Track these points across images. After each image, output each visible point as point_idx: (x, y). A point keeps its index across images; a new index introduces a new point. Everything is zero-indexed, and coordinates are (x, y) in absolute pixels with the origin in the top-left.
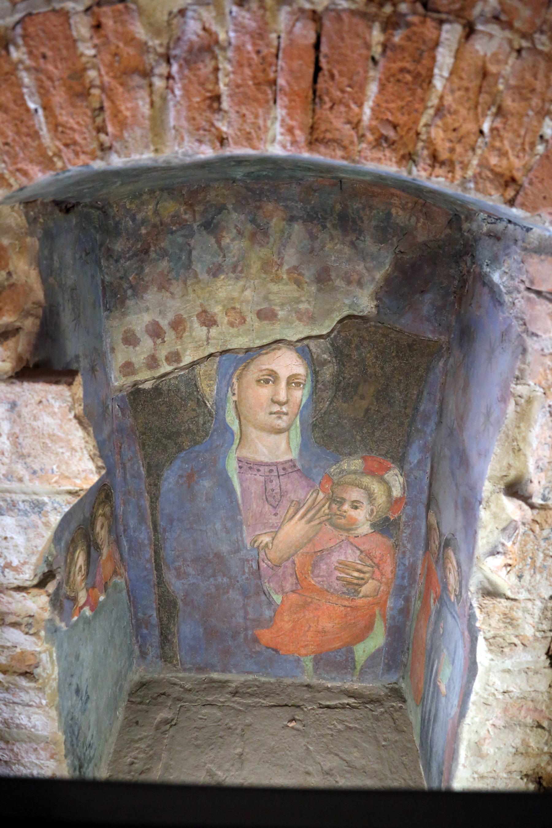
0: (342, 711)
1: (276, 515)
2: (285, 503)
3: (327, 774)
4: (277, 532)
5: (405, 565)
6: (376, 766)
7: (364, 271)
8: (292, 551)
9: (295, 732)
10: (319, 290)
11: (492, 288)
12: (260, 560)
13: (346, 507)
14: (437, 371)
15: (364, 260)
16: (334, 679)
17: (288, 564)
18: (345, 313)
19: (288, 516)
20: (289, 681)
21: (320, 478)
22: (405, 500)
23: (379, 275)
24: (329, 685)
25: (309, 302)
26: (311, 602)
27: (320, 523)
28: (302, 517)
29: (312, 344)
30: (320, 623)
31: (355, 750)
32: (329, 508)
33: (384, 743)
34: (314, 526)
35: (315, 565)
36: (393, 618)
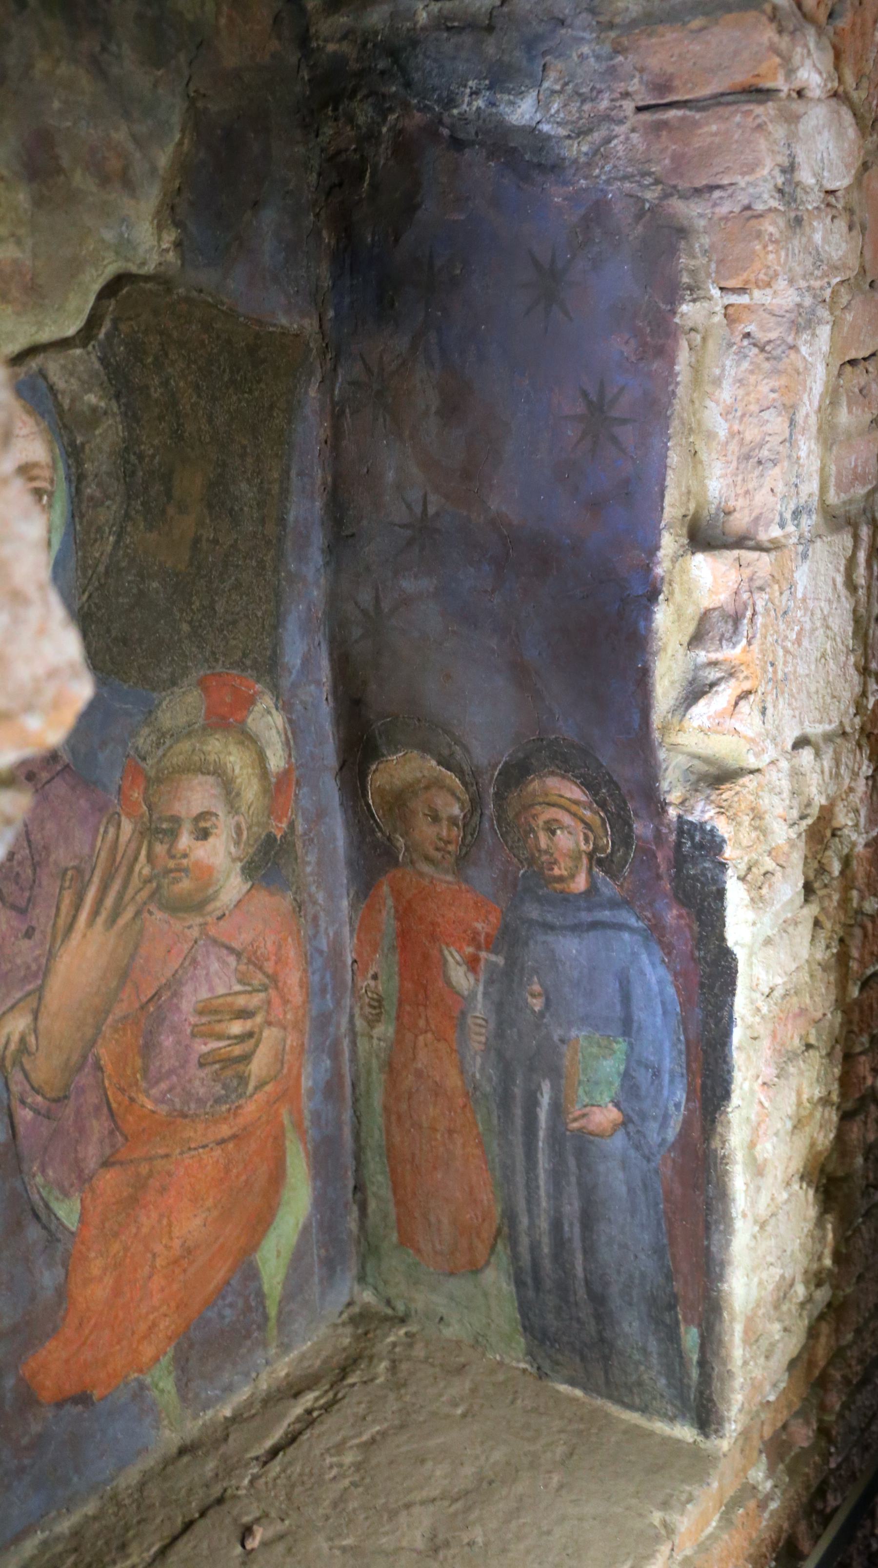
0: (317, 1430)
1: (29, 933)
2: (48, 885)
3: (436, 1550)
4: (41, 989)
5: (321, 952)
6: (498, 1455)
7: (131, 146)
8: (89, 1032)
9: (280, 1548)
10: (39, 202)
11: (525, 158)
12: (15, 1103)
13: (185, 841)
14: (307, 411)
15: (127, 115)
16: (229, 1389)
17: (85, 1078)
18: (111, 270)
19: (62, 922)
20: (131, 1476)
21: (118, 775)
22: (295, 775)
23: (163, 159)
24: (228, 1412)
25: (19, 242)
26: (150, 1175)
27: (138, 913)
28: (95, 913)
29: (53, 365)
30: (176, 1232)
31: (429, 1465)
32: (150, 858)
33: (459, 1411)
34: (126, 926)
35: (148, 1048)
36: (317, 1116)
